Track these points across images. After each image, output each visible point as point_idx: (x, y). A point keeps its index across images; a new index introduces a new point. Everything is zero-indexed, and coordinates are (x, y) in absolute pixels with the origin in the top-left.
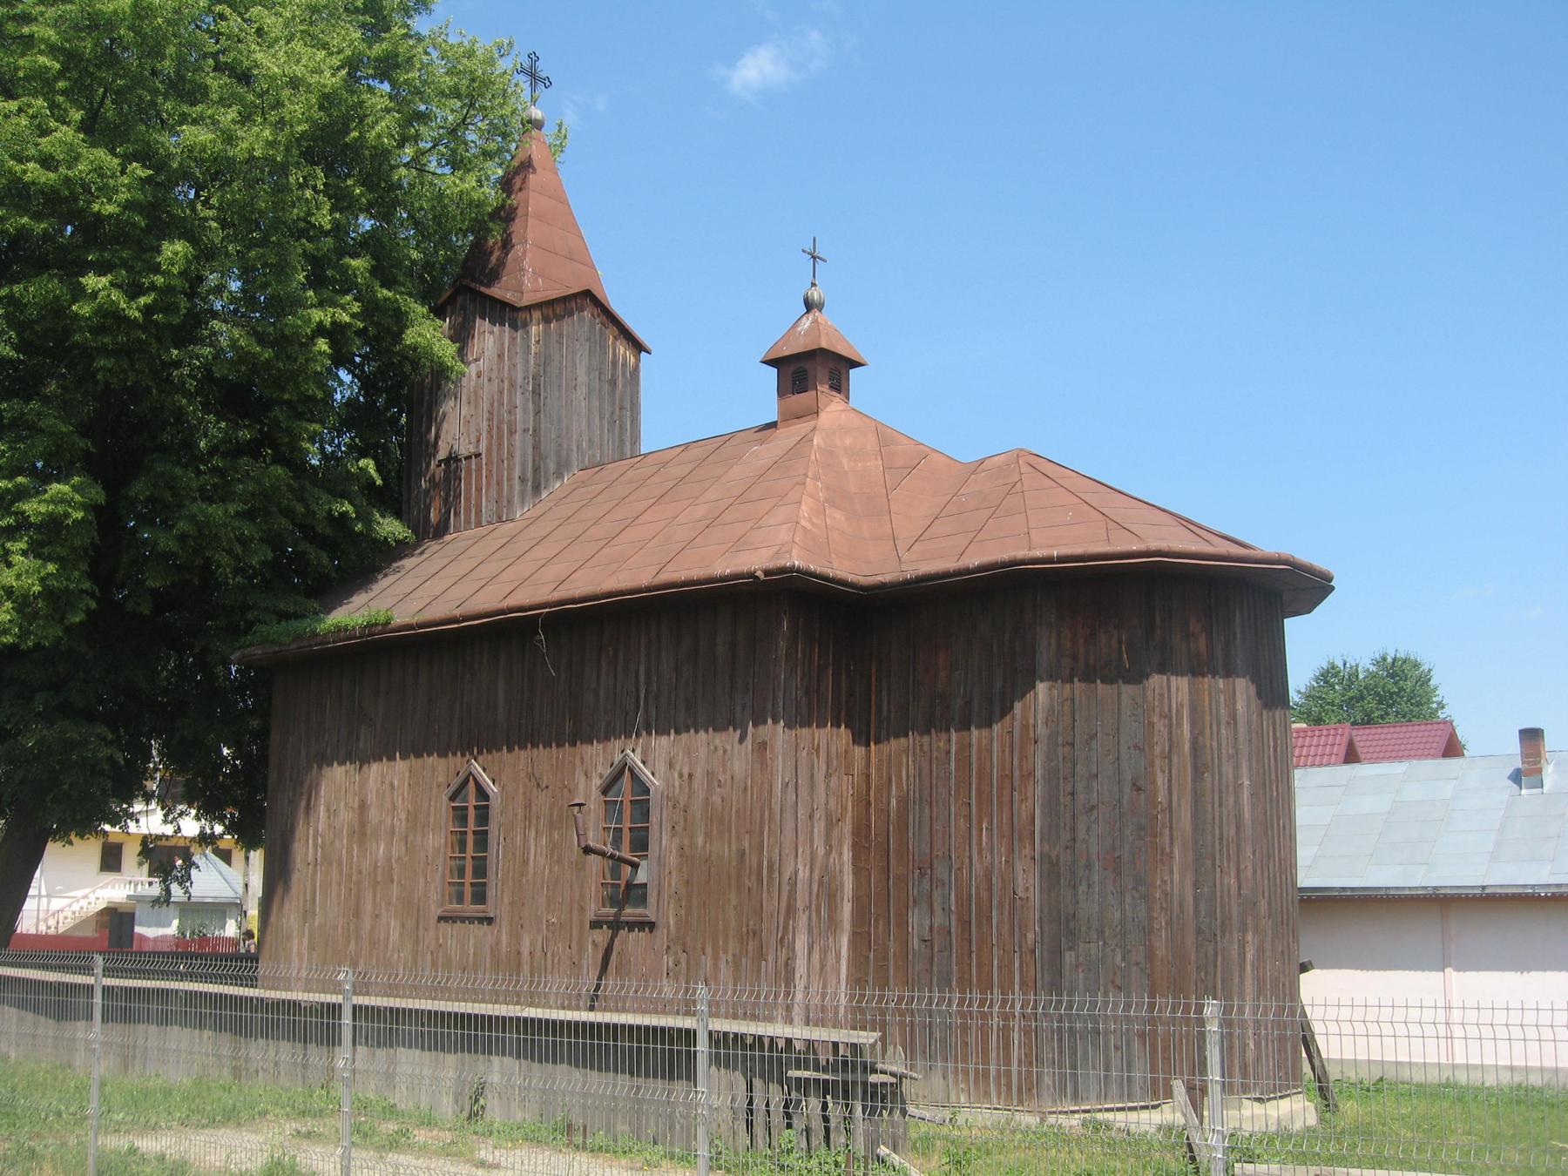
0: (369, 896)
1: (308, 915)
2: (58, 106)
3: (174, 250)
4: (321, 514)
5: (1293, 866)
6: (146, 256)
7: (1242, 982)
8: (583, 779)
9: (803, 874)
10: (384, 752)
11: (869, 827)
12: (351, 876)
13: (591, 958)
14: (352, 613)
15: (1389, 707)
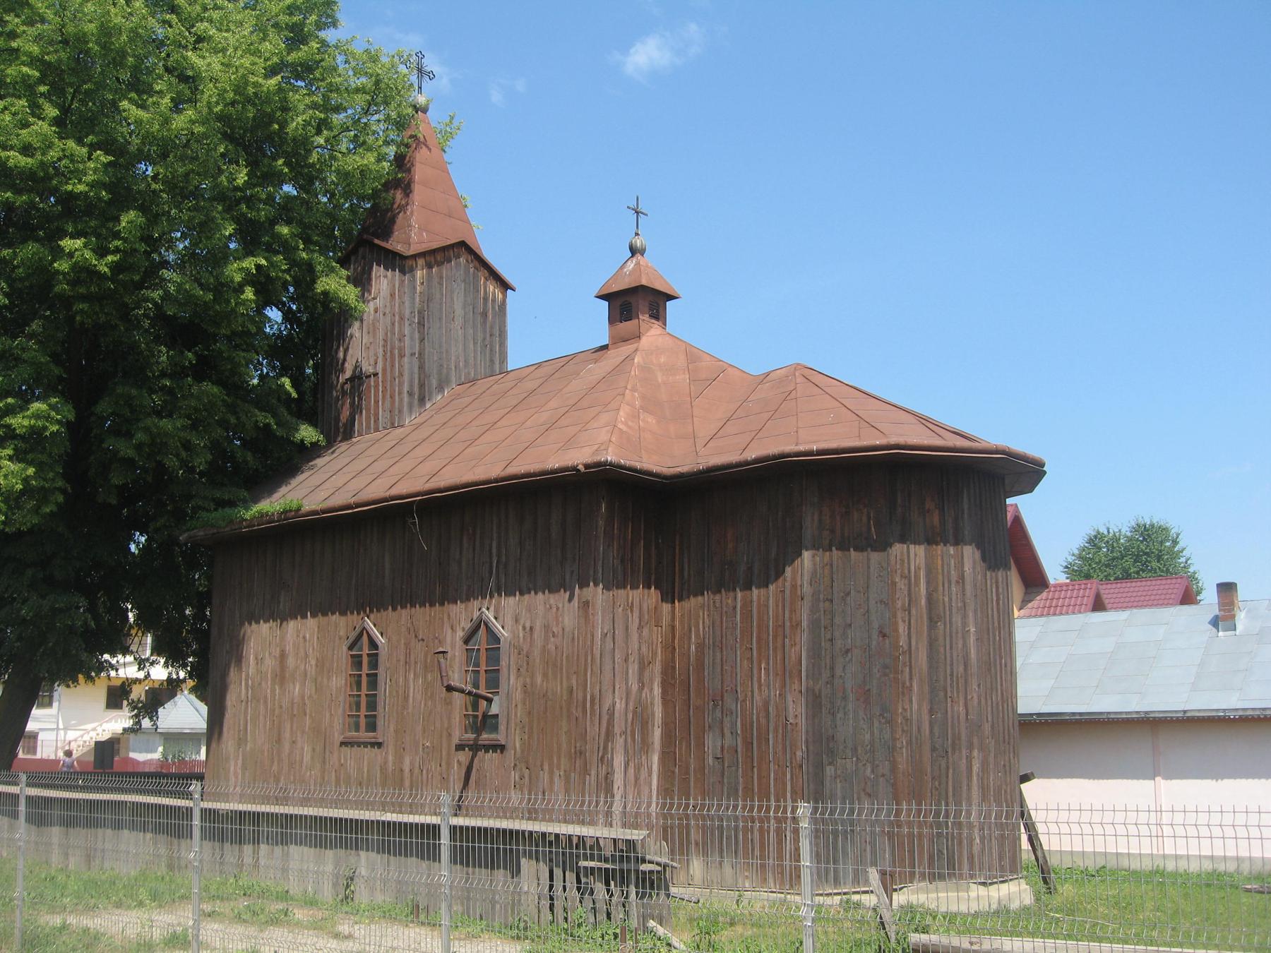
1: (241, 741)
3: (129, 218)
7: (969, 788)
8: (450, 631)
9: (620, 706)
10: (299, 612)
11: (674, 668)
13: (457, 773)
14: (272, 504)
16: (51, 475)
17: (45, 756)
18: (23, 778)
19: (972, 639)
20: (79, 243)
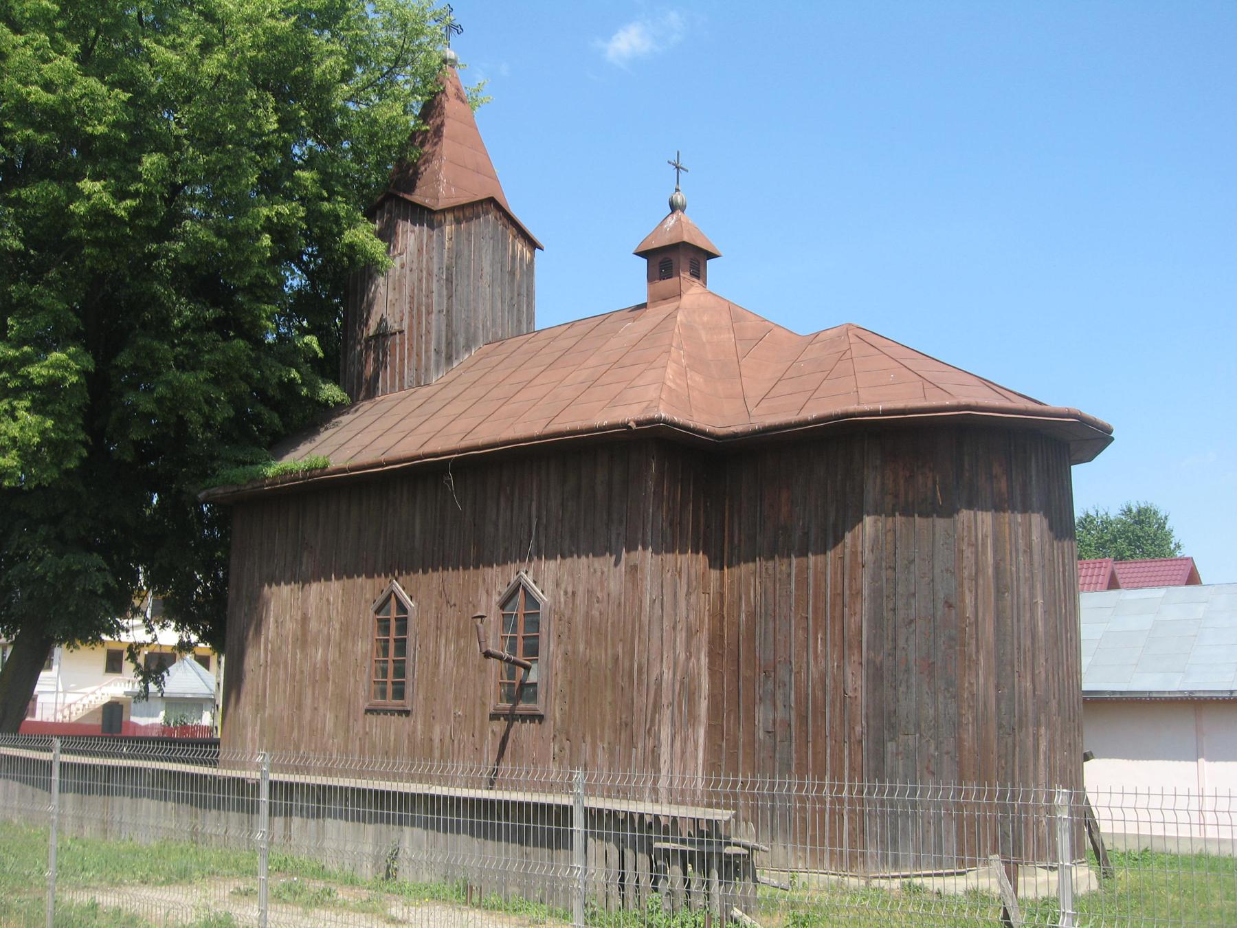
0: (309, 692)
1: (259, 707)
2: (57, 42)
4: (274, 381)
5: (1078, 672)
6: (131, 166)
9: (667, 676)
10: (322, 573)
11: (722, 637)
12: (294, 676)
14: (298, 459)
15: (1140, 545)
16: (71, 427)
17: (45, 719)
18: (57, 743)
19: (1040, 611)
20: (98, 186)
